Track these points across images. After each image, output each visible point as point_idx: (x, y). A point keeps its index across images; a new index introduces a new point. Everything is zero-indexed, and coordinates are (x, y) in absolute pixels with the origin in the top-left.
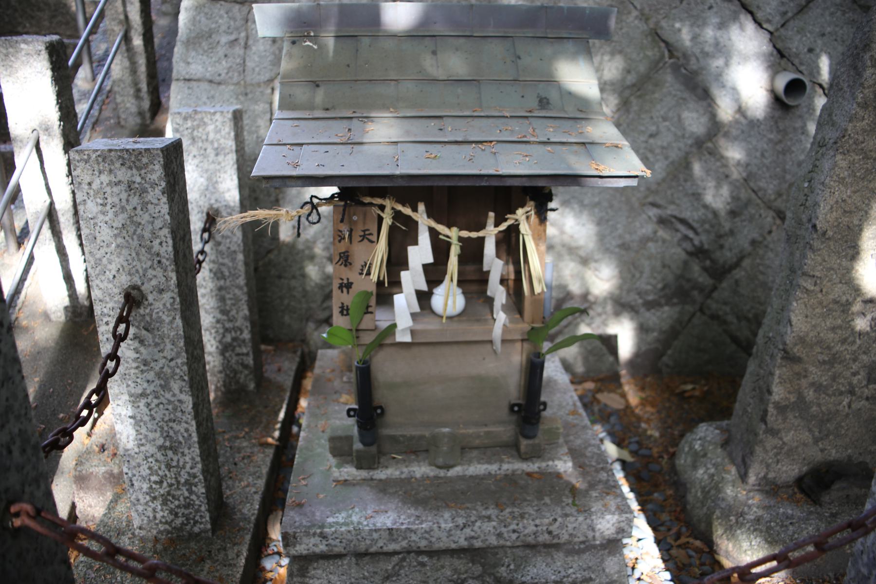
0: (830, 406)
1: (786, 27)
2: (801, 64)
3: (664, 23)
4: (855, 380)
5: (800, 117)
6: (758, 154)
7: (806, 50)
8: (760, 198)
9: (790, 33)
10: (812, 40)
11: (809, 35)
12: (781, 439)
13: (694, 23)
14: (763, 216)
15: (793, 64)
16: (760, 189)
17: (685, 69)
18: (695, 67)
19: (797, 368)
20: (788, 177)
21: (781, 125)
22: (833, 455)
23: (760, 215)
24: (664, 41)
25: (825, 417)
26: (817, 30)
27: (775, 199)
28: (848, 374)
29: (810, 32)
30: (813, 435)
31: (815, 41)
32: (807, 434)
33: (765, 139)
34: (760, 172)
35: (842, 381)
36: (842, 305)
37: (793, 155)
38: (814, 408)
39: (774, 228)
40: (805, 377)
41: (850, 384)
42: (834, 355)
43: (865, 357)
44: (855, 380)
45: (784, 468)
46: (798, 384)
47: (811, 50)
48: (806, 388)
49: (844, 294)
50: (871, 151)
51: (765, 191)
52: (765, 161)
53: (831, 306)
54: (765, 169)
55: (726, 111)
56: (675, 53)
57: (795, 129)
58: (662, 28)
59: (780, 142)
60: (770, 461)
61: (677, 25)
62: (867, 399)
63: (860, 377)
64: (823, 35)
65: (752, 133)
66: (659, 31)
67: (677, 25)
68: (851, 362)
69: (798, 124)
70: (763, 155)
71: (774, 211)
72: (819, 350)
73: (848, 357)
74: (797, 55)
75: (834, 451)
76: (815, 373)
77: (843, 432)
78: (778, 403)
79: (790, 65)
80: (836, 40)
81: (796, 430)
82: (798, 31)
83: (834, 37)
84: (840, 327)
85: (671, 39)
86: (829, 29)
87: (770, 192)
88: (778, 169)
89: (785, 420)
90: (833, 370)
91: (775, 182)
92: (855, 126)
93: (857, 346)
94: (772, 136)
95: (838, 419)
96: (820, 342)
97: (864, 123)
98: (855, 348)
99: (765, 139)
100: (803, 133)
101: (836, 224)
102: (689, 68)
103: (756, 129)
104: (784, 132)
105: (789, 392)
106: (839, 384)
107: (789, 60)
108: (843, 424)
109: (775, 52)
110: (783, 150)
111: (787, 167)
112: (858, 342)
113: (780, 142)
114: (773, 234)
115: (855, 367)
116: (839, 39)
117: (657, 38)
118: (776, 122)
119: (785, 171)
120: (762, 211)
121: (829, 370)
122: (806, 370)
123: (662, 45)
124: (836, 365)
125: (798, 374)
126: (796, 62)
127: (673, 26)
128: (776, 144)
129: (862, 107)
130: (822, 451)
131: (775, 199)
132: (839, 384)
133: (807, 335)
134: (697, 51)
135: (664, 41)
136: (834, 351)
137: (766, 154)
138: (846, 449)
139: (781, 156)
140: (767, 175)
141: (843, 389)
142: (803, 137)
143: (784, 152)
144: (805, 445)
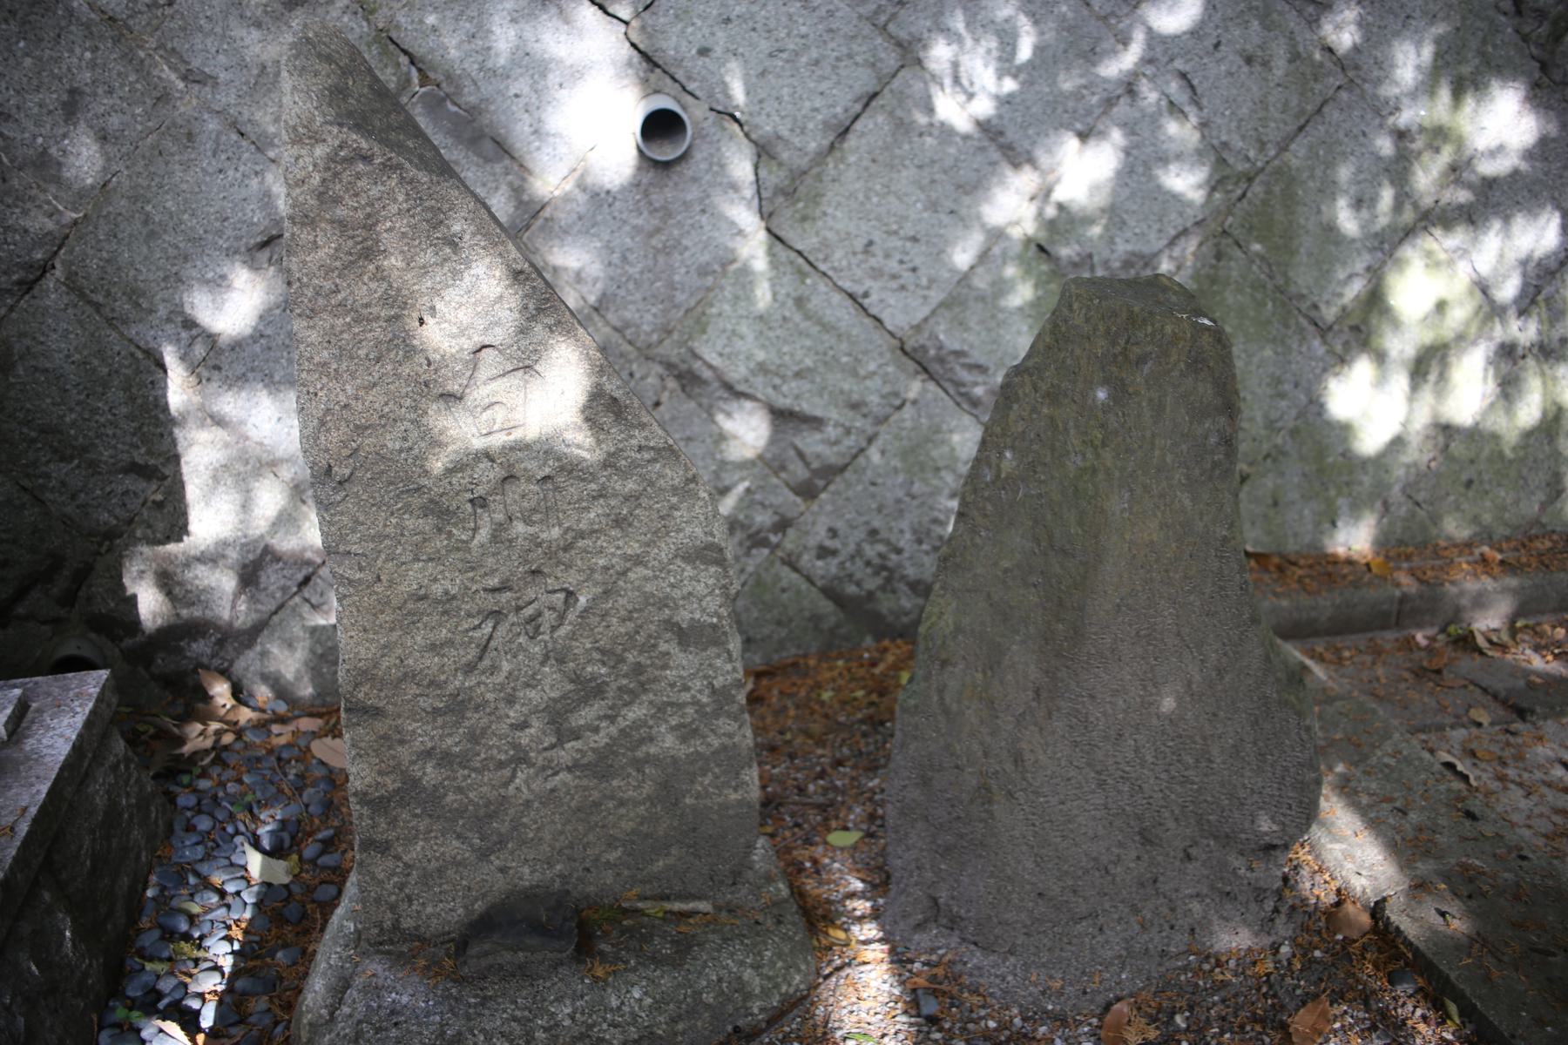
0: (484, 789)
1: (652, 9)
2: (689, 78)
3: (401, 19)
4: (524, 738)
5: (695, 180)
6: (615, 258)
7: (694, 51)
8: (630, 343)
9: (662, 20)
10: (706, 31)
11: (699, 23)
12: (398, 858)
13: (462, 13)
14: (637, 376)
15: (675, 80)
16: (627, 325)
17: (455, 104)
18: (472, 99)
19: (381, 726)
20: (680, 297)
21: (657, 198)
22: (527, 877)
23: (631, 375)
24: (405, 52)
25: (482, 812)
26: (715, 12)
27: (661, 342)
28: (504, 728)
29: (699, 16)
30: (471, 846)
31: (713, 34)
32: (456, 843)
33: (627, 228)
34: (622, 292)
35: (493, 741)
36: (438, 602)
37: (687, 254)
38: (451, 797)
39: (665, 397)
40: (402, 742)
41: (516, 746)
42: (454, 696)
43: (532, 694)
44: (524, 738)
45: (429, 910)
46: (394, 757)
47: (704, 52)
48: (413, 763)
49: (435, 580)
50: (367, 306)
51: (638, 326)
52: (631, 270)
53: (410, 606)
54: (631, 286)
55: (551, 180)
56: (432, 75)
57: (687, 205)
58: (398, 27)
59: (658, 230)
60: (393, 898)
61: (431, 19)
62: (569, 769)
63: (532, 731)
64: (728, 20)
65: (599, 218)
66: (394, 35)
67: (431, 19)
68: (502, 705)
69: (693, 194)
70: (624, 259)
71: (661, 363)
72: (414, 690)
73: (490, 696)
74: (679, 62)
75: (526, 870)
76: (423, 734)
77: (531, 835)
78: (366, 794)
79: (668, 81)
80: (754, 29)
81: (425, 839)
82: (677, 16)
83: (751, 24)
84: (450, 643)
85: (419, 49)
86: (738, 10)
87: (646, 328)
88: (658, 284)
89: (393, 823)
90: (467, 723)
91: (654, 310)
92: (304, 262)
93: (504, 674)
94: (640, 221)
95: (512, 811)
96: (409, 676)
97: (321, 253)
98: (500, 678)
99: (627, 228)
100: (703, 211)
101: (346, 452)
102: (462, 101)
103: (605, 209)
104: (666, 213)
105: (380, 773)
106: (491, 747)
107: (665, 72)
108: (525, 820)
109: (636, 57)
110: (665, 247)
111: (677, 278)
112: (506, 666)
113: (658, 230)
114: (662, 408)
115: (514, 714)
116: (758, 26)
117: (392, 47)
118: (646, 194)
119: (672, 286)
120: (635, 367)
121: (457, 724)
122: (398, 730)
123: (404, 60)
124: (469, 714)
125: (385, 737)
126: (680, 75)
127: (421, 22)
128: (651, 235)
129: (303, 224)
130: (503, 870)
131: (661, 342)
132: (491, 747)
133: (376, 665)
134: (472, 67)
135: (405, 52)
136: (450, 688)
137: (631, 257)
138: (551, 865)
139: (661, 259)
140: (638, 296)
141: (503, 757)
142: (704, 219)
143: (666, 250)
144: (458, 864)
